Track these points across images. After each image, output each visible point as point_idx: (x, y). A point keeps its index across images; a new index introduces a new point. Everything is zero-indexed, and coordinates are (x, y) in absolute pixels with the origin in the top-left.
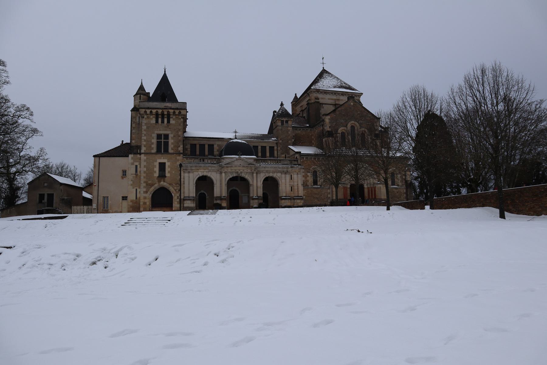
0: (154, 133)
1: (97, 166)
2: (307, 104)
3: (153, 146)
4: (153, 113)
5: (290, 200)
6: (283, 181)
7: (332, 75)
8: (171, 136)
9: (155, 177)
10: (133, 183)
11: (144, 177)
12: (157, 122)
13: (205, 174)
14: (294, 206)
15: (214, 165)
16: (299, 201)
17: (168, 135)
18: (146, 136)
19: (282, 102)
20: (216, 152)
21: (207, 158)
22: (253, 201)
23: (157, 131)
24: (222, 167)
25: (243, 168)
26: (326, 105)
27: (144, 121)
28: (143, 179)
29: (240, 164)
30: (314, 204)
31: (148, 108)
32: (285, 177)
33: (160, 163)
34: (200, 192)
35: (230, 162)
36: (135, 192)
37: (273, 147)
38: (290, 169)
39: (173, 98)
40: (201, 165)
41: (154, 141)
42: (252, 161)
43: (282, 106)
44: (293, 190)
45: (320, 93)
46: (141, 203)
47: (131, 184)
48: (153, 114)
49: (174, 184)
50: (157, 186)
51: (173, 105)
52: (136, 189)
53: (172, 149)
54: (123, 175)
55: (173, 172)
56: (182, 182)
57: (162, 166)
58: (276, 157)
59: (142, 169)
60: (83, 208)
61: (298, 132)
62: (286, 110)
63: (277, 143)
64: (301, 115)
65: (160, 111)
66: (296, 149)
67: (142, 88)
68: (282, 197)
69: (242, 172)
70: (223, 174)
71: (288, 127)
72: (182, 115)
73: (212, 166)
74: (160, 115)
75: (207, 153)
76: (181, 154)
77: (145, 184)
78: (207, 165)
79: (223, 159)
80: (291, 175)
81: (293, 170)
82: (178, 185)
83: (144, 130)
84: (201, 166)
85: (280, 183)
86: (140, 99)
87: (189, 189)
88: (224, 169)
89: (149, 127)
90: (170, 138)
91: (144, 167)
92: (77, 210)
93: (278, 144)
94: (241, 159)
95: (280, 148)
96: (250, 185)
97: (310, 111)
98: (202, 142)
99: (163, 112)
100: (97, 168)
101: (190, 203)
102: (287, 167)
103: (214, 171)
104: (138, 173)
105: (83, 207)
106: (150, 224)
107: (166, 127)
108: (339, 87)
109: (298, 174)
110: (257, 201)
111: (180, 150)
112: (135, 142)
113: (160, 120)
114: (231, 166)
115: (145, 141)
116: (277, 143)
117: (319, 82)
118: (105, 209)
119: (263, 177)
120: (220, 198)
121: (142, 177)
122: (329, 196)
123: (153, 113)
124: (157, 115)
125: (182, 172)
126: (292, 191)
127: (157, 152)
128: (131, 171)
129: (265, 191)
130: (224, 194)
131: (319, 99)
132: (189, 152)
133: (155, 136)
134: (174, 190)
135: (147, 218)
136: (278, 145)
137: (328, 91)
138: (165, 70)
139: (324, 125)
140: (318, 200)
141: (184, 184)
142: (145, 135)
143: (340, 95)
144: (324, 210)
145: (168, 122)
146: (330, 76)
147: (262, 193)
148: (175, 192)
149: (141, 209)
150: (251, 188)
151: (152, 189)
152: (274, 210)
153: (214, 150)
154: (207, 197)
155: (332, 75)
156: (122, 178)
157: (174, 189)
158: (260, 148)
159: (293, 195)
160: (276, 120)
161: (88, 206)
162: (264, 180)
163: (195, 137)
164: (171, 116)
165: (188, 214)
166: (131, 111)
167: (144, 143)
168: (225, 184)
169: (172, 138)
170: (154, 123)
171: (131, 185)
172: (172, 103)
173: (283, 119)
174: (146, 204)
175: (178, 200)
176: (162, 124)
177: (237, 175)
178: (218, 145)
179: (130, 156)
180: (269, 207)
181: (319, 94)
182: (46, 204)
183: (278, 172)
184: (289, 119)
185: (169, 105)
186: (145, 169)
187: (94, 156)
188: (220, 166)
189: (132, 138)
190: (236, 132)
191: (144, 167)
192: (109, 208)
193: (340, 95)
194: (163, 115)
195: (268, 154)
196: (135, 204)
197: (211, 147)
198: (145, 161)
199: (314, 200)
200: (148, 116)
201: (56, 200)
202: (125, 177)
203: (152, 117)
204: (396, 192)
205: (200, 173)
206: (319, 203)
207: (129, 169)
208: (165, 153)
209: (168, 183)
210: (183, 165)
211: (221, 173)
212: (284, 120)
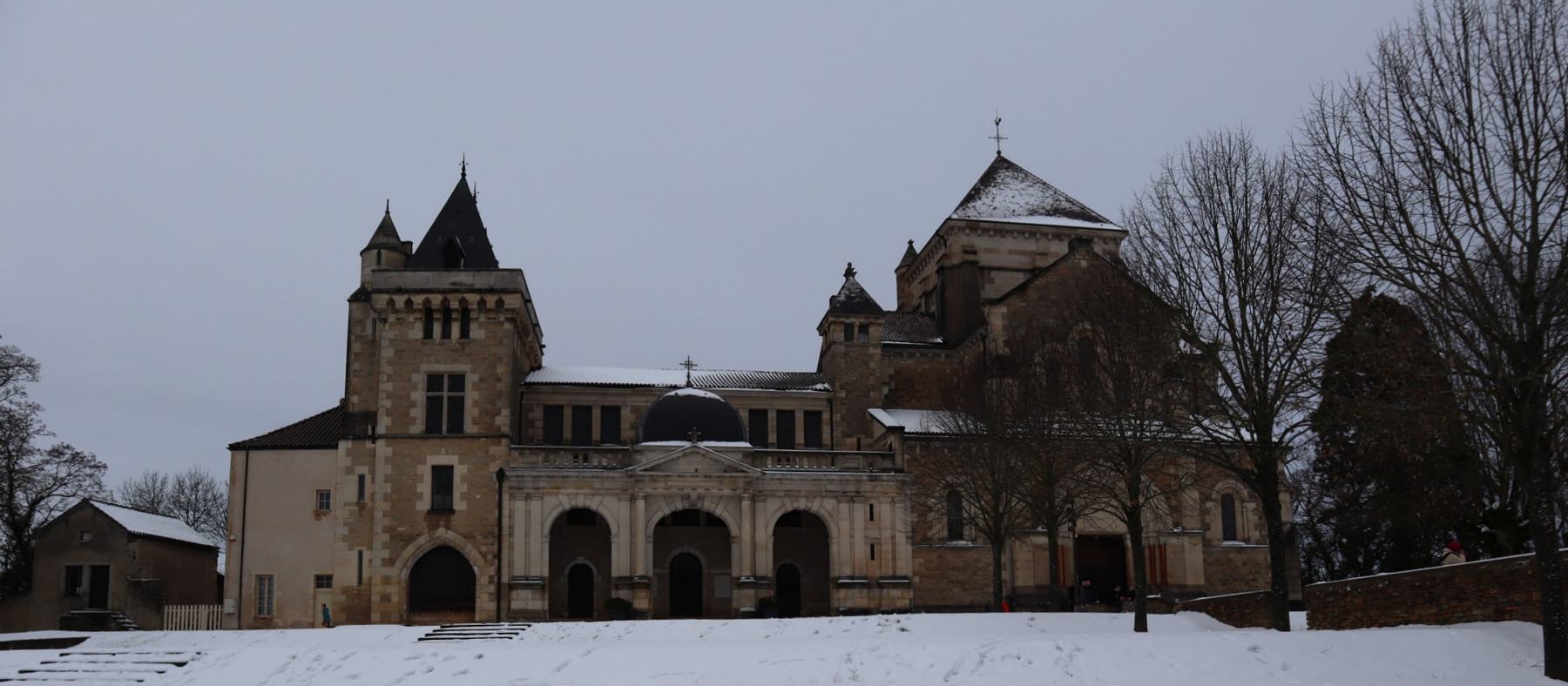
0: (417, 371)
1: (241, 479)
2: (937, 272)
3: (414, 412)
4: (415, 307)
5: (866, 591)
6: (844, 525)
7: (1027, 174)
8: (471, 379)
9: (419, 512)
10: (349, 532)
11: (384, 512)
12: (428, 334)
13: (581, 502)
14: (882, 608)
15: (611, 474)
16: (896, 593)
18: (392, 381)
19: (850, 265)
20: (626, 432)
21: (596, 451)
22: (741, 591)
23: (429, 362)
24: (636, 481)
25: (705, 481)
26: (1002, 274)
27: (388, 333)
28: (380, 521)
29: (696, 470)
30: (949, 603)
31: (400, 291)
32: (851, 512)
33: (435, 468)
35: (662, 461)
36: (356, 560)
37: (819, 413)
38: (867, 487)
39: (483, 257)
40: (569, 474)
41: (419, 396)
42: (735, 459)
43: (851, 278)
44: (876, 557)
46: (375, 598)
48: (415, 311)
49: (479, 537)
50: (424, 542)
51: (482, 279)
52: (360, 553)
53: (475, 422)
54: (321, 507)
55: (478, 497)
56: (505, 530)
57: (443, 476)
58: (828, 445)
59: (379, 488)
60: (198, 613)
61: (906, 362)
62: (862, 290)
63: (830, 401)
64: (923, 309)
65: (436, 300)
66: (887, 418)
67: (387, 228)
68: (840, 578)
69: (704, 496)
70: (641, 504)
71: (867, 346)
72: (507, 310)
73: (602, 477)
74: (438, 310)
75: (596, 434)
76: (505, 436)
77: (388, 535)
78: (588, 473)
79: (641, 452)
80: (871, 506)
81: (877, 489)
82: (491, 540)
83: (388, 362)
84: (568, 477)
86: (379, 262)
87: (527, 554)
88: (641, 485)
89: (401, 351)
90: (468, 386)
91: (386, 481)
92: (178, 619)
93: (834, 403)
94: (698, 453)
95: (839, 415)
97: (947, 294)
98: (582, 400)
100: (240, 483)
101: (530, 596)
102: (858, 478)
103: (609, 491)
104: (365, 501)
105: (198, 608)
106: (103, 675)
107: (456, 350)
108: (1048, 213)
109: (893, 502)
110: (751, 592)
111: (500, 423)
112: (361, 401)
113: (437, 329)
114: (666, 476)
115: (389, 396)
116: (830, 401)
117: (980, 199)
118: (263, 616)
119: (776, 511)
120: (629, 582)
121: (378, 514)
123: (415, 307)
125: (506, 497)
126: (873, 558)
130: (644, 566)
131: (975, 253)
132: (540, 433)
133: (419, 379)
134: (478, 556)
135: (114, 654)
136: (834, 408)
137: (1006, 227)
138: (464, 169)
139: (986, 336)
140: (964, 590)
141: (511, 534)
142: (390, 378)
143: (1050, 237)
144: (906, 627)
145: (465, 333)
146: (1020, 179)
149: (375, 616)
150: (734, 547)
151: (410, 552)
152: (726, 624)
153: (623, 426)
154: (595, 580)
155: (1026, 175)
156: (318, 515)
157: (481, 552)
158: (772, 415)
159: (877, 574)
160: (829, 325)
161: (211, 607)
163: (559, 384)
164: (473, 315)
165: (423, 637)
166: (349, 301)
167: (387, 403)
168: (647, 537)
169: (476, 387)
170: (418, 340)
171: (345, 538)
172: (477, 273)
173: (851, 320)
174: (390, 601)
175: (492, 588)
176: (446, 341)
177: (687, 506)
178: (635, 410)
179: (344, 445)
180: (803, 612)
181: (979, 235)
182: (86, 599)
183: (826, 496)
184: (872, 320)
185: (464, 278)
186: (388, 488)
187: (233, 447)
188: (630, 476)
189: (351, 388)
190: (689, 365)
191: (386, 481)
192: (275, 613)
193: (1050, 237)
194: (446, 311)
195: (800, 437)
196: (356, 601)
197: (611, 415)
198: (388, 460)
199: (951, 590)
200: (399, 316)
201: (116, 585)
202: (325, 514)
203: (413, 320)
204: (1240, 564)
205: (566, 500)
206: (967, 600)
207: (338, 486)
208: (451, 435)
209: (460, 534)
210: (507, 473)
211: (633, 499)
212: (854, 323)
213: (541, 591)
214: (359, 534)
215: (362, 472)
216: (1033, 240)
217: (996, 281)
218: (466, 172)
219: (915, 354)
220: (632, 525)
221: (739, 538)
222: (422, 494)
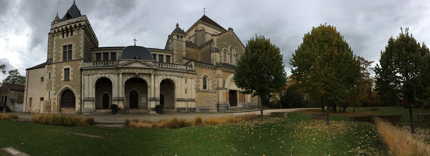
6: (179, 84)
11: (54, 81)
12: (63, 37)
17: (72, 45)
19: (177, 23)
30: (204, 106)
31: (56, 28)
33: (65, 69)
34: (104, 93)
45: (205, 25)
46: (52, 103)
47: (46, 88)
49: (76, 87)
51: (78, 19)
52: (49, 92)
53: (74, 56)
55: (75, 76)
57: (67, 70)
65: (64, 28)
80: (186, 79)
85: (176, 86)
91: (55, 74)
95: (175, 57)
96: (148, 86)
99: (66, 27)
121: (53, 82)
122: (215, 99)
124: (63, 30)
127: (64, 60)
128: (46, 77)
129: (162, 93)
133: (61, 48)
147: (159, 95)
148: (77, 93)
150: (149, 89)
154: (109, 98)
157: (76, 91)
162: (161, 83)
171: (46, 88)
185: (74, 20)
186: (55, 75)
187: (26, 70)
191: (55, 74)
198: (55, 68)
209: (71, 86)
211: (119, 74)
213: (92, 102)
214: (49, 87)
215: (50, 72)
216: (215, 29)
217: (208, 35)
218: (75, 2)
219: (191, 47)
220: (118, 82)
221: (151, 86)
222: (62, 76)
